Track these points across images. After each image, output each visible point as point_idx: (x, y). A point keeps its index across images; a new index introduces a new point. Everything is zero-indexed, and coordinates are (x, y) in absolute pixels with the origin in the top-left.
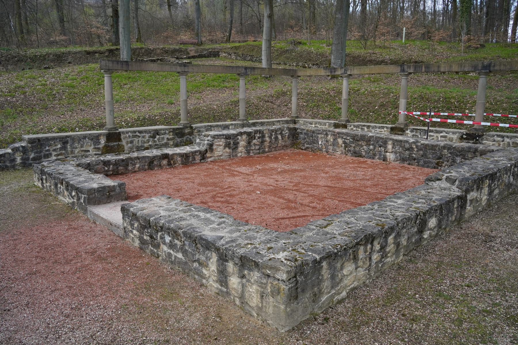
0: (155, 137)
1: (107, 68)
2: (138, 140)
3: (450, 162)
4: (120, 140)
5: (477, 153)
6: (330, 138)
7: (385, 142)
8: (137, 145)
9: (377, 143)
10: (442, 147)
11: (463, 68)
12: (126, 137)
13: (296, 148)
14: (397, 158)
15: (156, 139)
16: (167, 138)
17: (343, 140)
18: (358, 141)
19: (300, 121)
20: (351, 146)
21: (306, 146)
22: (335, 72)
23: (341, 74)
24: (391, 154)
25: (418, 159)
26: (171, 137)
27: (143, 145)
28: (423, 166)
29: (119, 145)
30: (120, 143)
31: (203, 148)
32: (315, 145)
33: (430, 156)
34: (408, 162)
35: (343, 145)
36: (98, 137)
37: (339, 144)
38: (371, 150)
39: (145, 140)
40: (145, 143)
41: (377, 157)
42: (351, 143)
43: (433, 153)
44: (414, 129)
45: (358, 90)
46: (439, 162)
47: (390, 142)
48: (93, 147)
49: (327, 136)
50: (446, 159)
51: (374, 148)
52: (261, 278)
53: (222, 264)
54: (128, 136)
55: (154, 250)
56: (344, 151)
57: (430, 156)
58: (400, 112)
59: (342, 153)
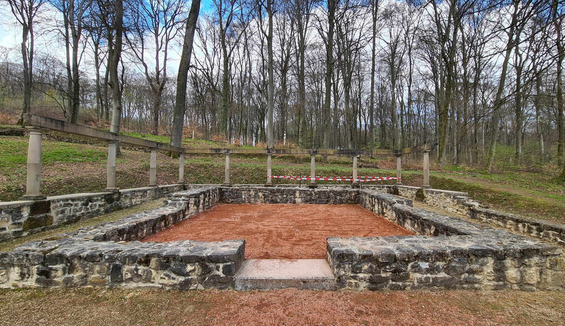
0: (88, 205)
1: (39, 125)
2: (71, 209)
4: (48, 210)
7: (294, 192)
8: (69, 214)
12: (56, 207)
14: (303, 200)
15: (88, 207)
16: (99, 205)
18: (274, 193)
21: (231, 200)
22: (219, 151)
26: (103, 203)
27: (74, 214)
28: (319, 204)
29: (47, 216)
30: (48, 214)
31: (183, 207)
36: (19, 209)
39: (78, 208)
40: (78, 211)
47: (298, 192)
48: (11, 222)
52: (541, 260)
53: (500, 263)
54: (59, 205)
55: (398, 283)
56: (263, 200)
59: (262, 202)
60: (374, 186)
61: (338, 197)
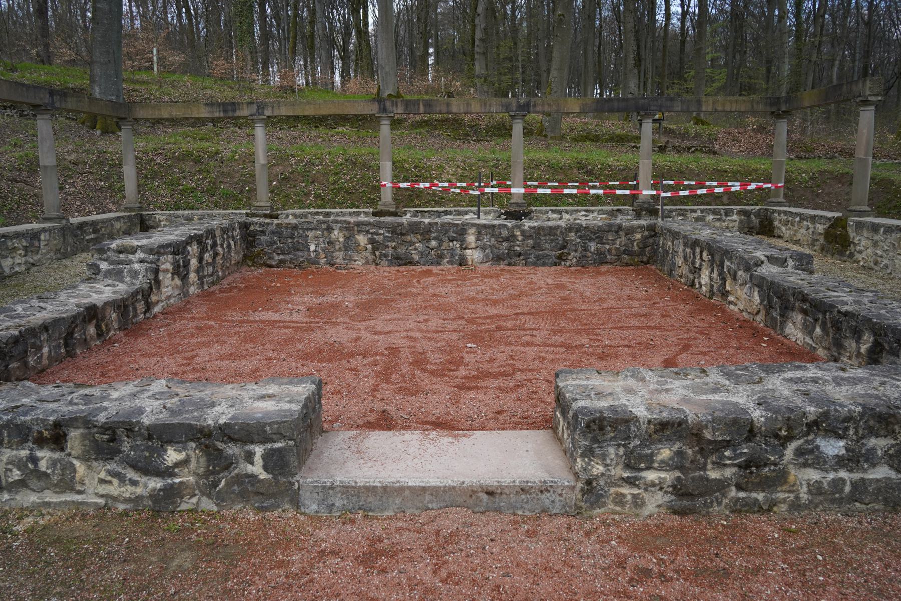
3: (579, 252)
5: (621, 233)
6: (337, 235)
7: (462, 231)
9: (445, 234)
10: (566, 229)
11: (488, 107)
13: (253, 265)
14: (487, 256)
17: (370, 236)
18: (402, 234)
19: (157, 217)
20: (387, 247)
21: (277, 258)
22: (234, 111)
23: (251, 115)
24: (474, 251)
25: (525, 254)
32: (300, 254)
33: (547, 246)
34: (506, 262)
35: (369, 246)
37: (359, 245)
38: (432, 249)
41: (446, 260)
42: (388, 241)
43: (552, 241)
44: (417, 212)
45: (217, 153)
46: (563, 253)
47: (472, 231)
49: (330, 233)
50: (573, 248)
51: (440, 245)
56: (371, 257)
57: (547, 246)
58: (385, 185)
59: (367, 263)
60: (702, 211)
61: (593, 246)
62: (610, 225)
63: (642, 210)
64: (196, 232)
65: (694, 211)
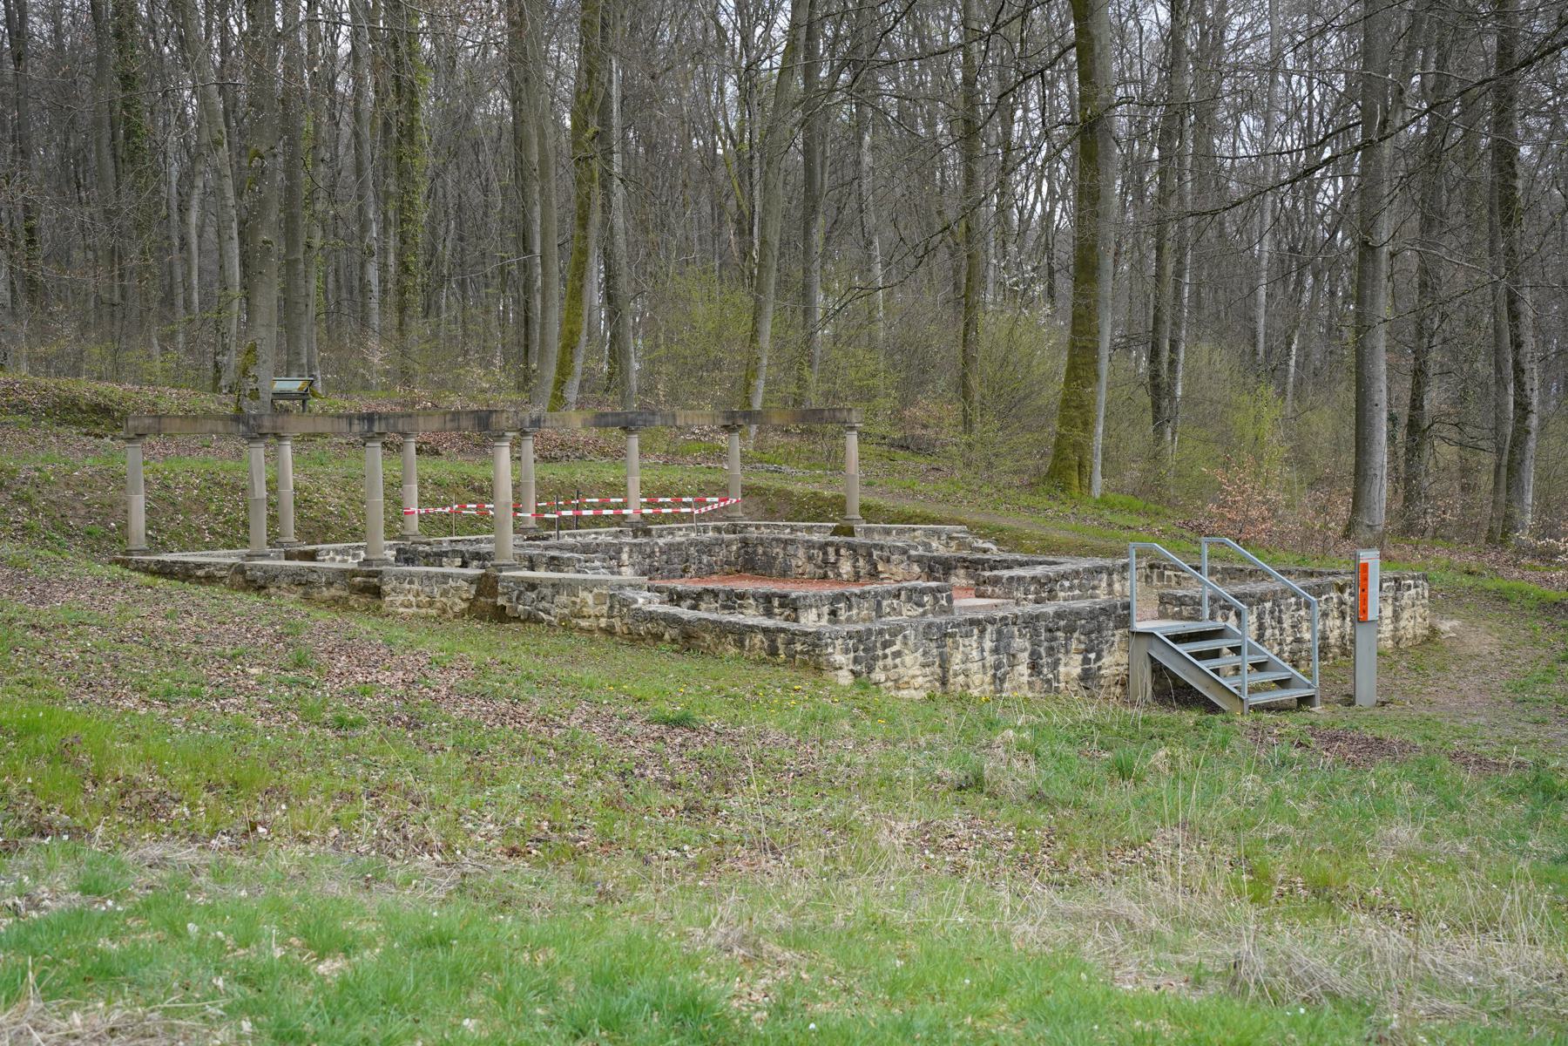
47: (626, 549)
60: (687, 529)
61: (705, 559)
62: (717, 539)
63: (637, 529)
64: (1384, 491)
65: (680, 529)
